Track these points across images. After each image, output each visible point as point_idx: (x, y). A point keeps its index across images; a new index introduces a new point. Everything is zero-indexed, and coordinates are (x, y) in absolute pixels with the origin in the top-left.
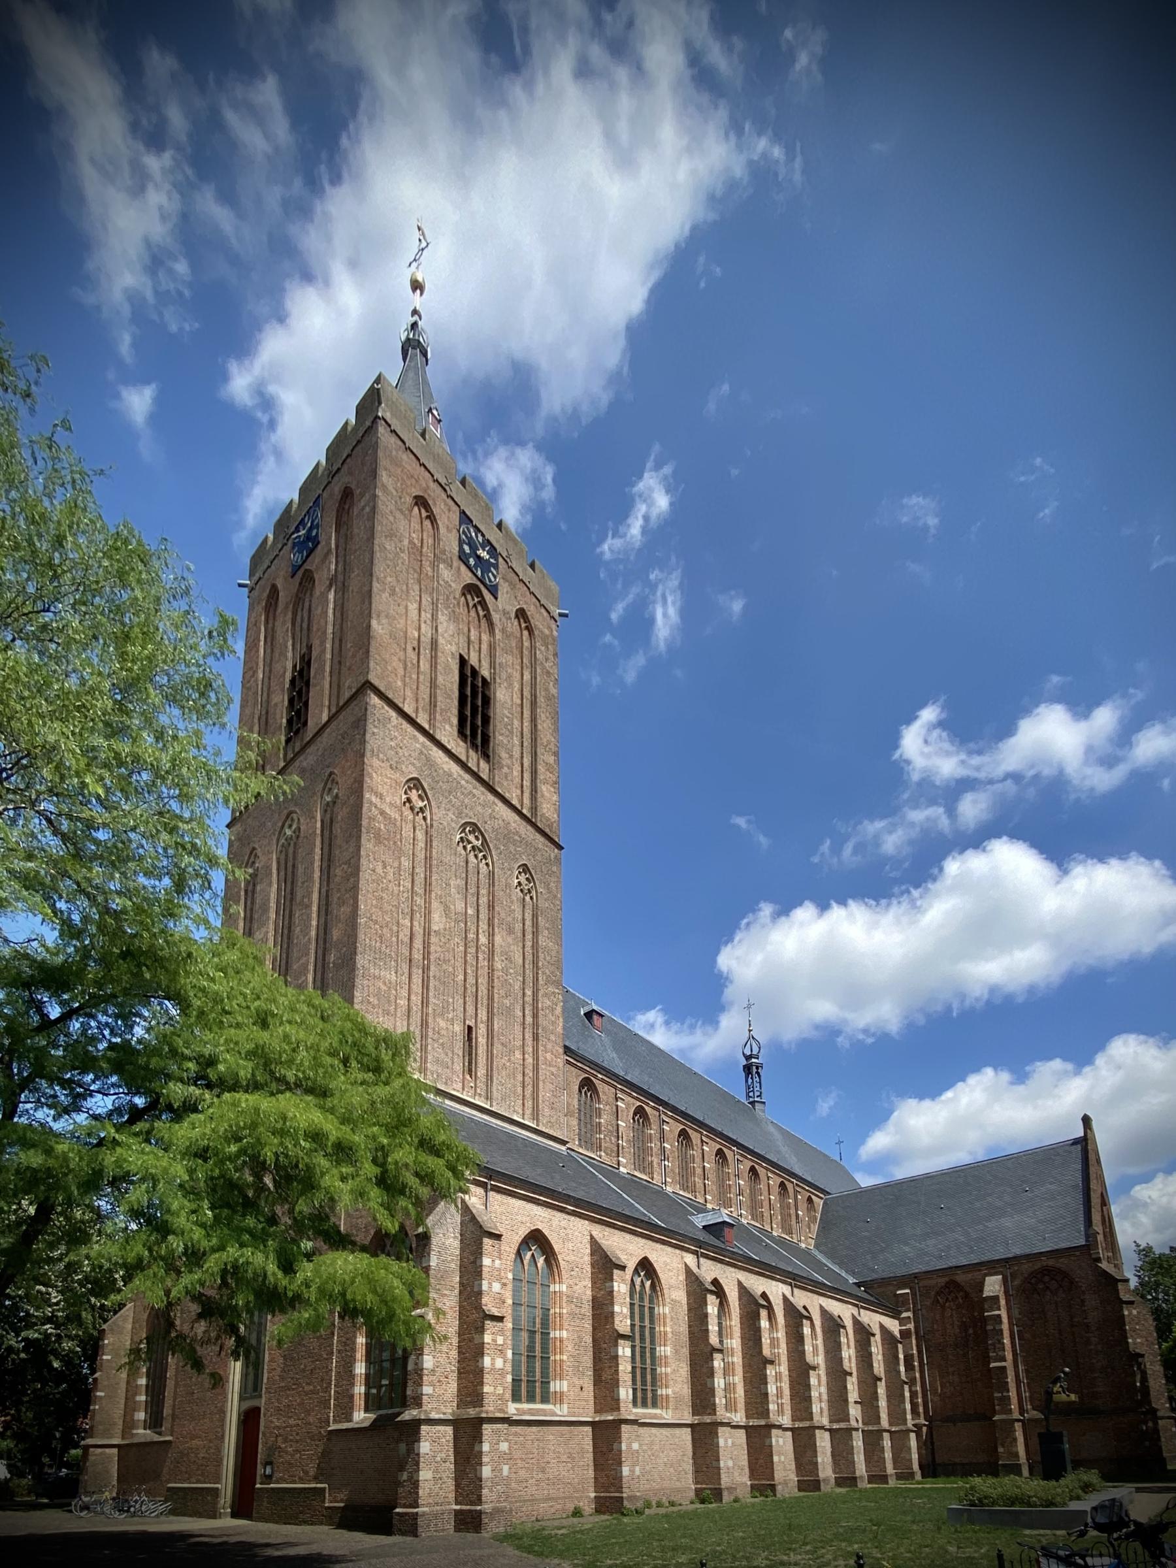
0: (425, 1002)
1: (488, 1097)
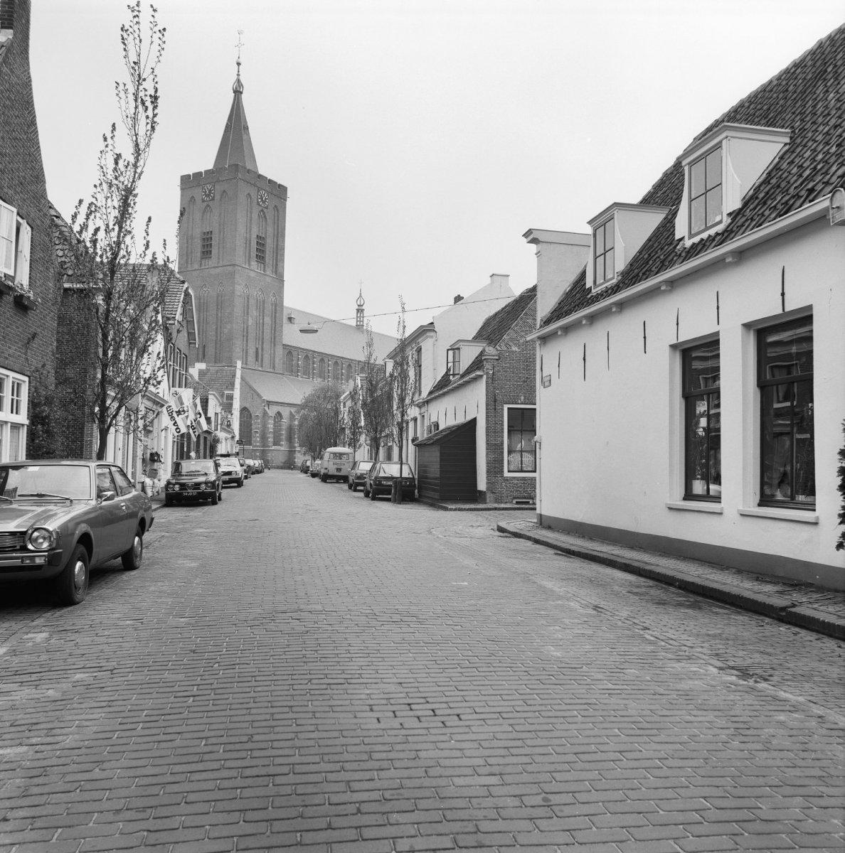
0: (247, 346)
1: (262, 366)
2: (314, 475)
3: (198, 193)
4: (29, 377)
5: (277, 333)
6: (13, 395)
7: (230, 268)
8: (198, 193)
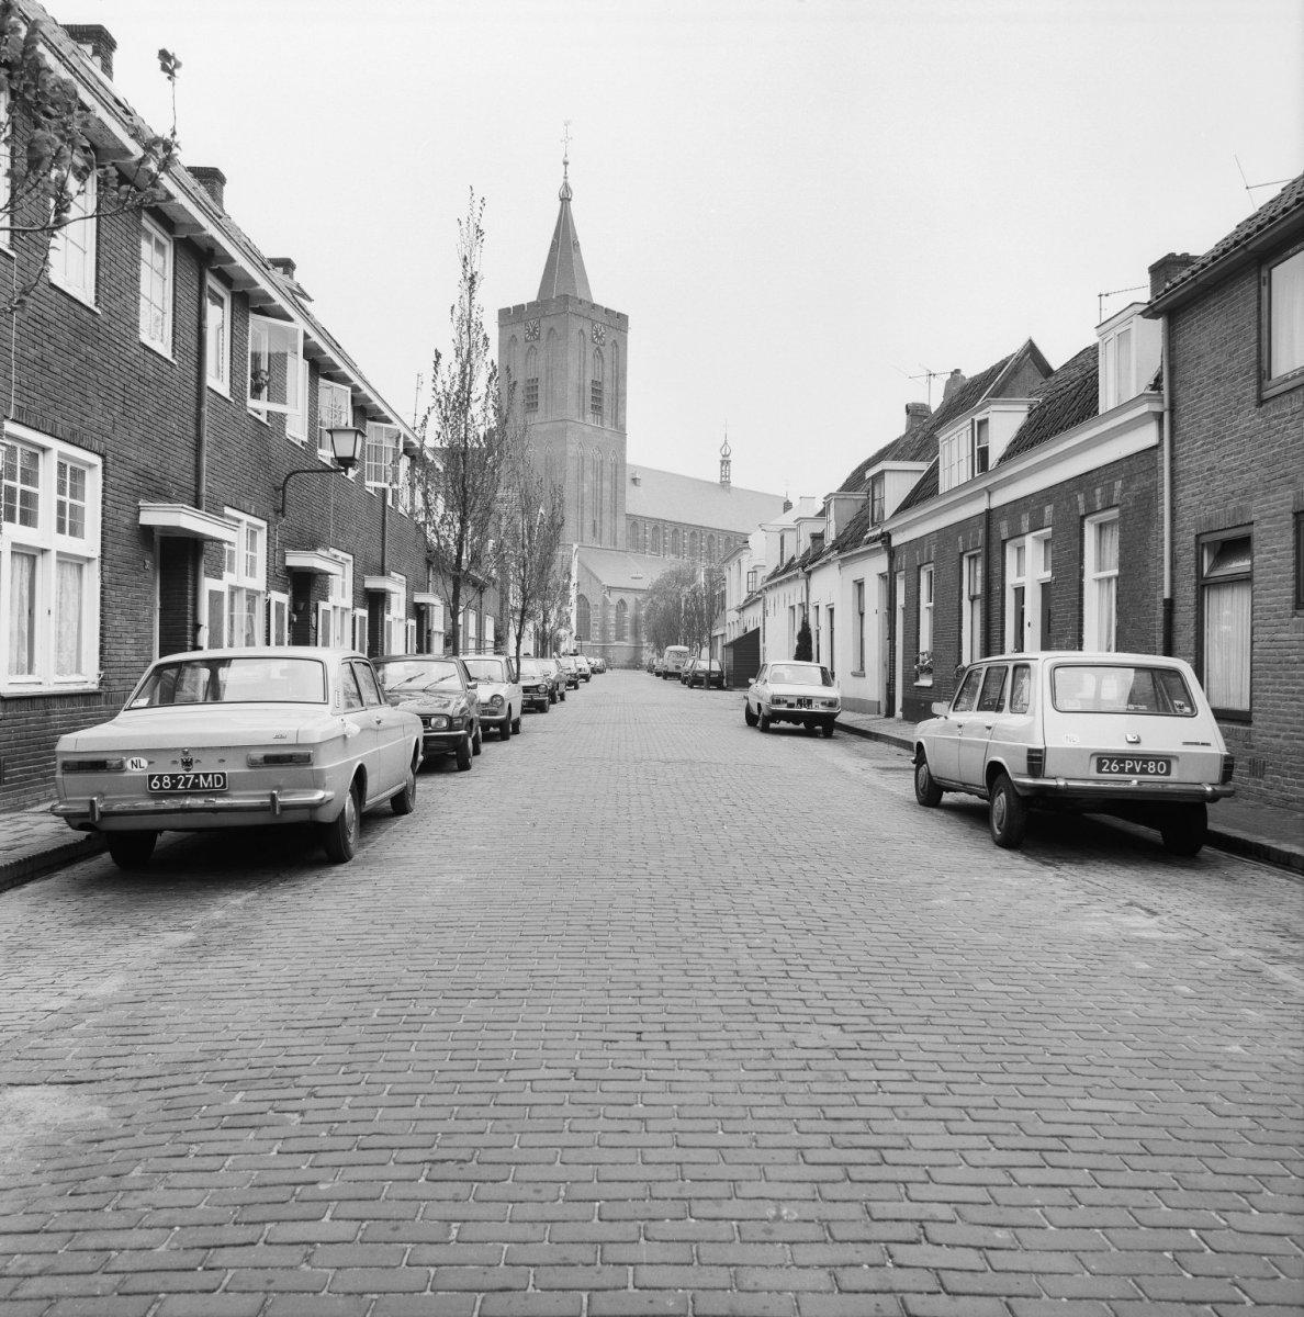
2: (658, 674)
3: (520, 331)
4: (103, 456)
5: (619, 494)
6: (61, 491)
7: (560, 424)
8: (520, 331)
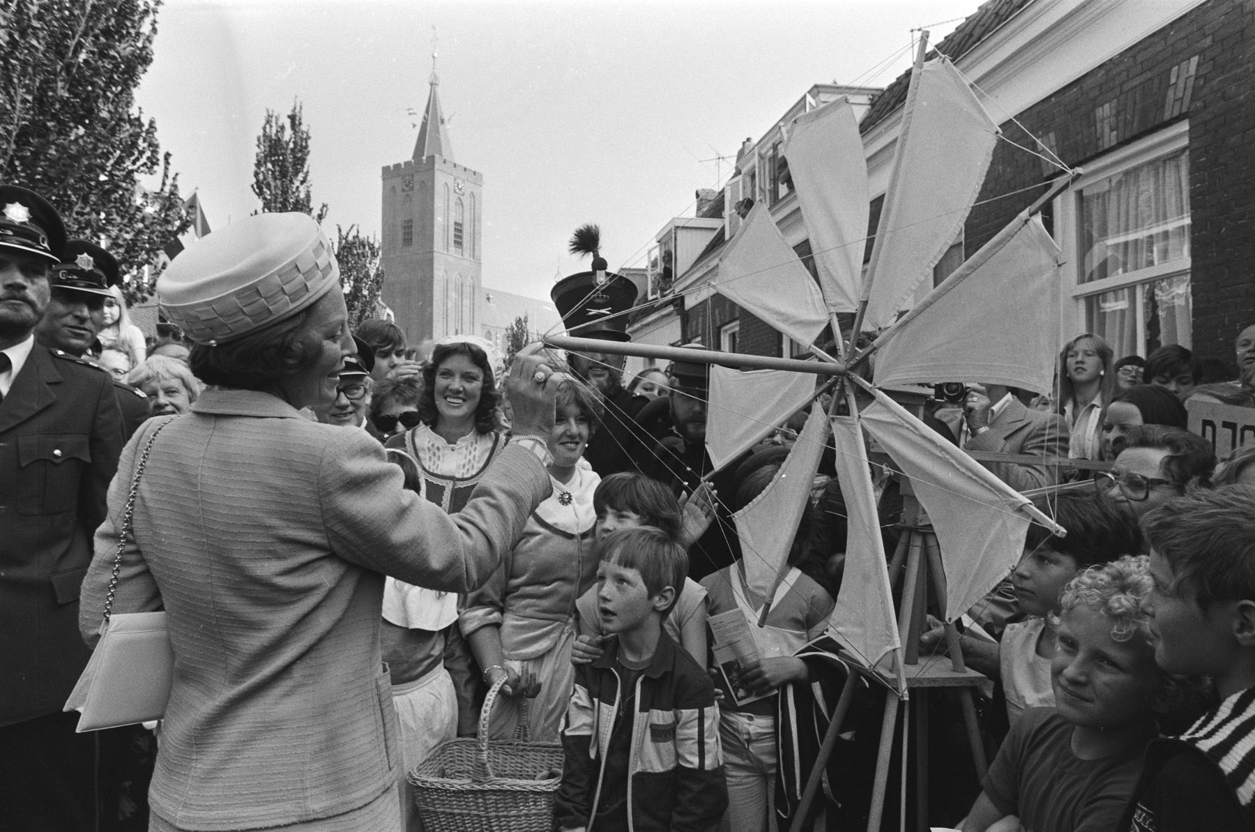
3: (397, 182)
